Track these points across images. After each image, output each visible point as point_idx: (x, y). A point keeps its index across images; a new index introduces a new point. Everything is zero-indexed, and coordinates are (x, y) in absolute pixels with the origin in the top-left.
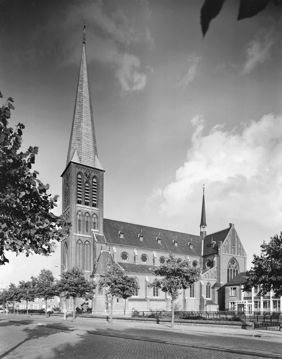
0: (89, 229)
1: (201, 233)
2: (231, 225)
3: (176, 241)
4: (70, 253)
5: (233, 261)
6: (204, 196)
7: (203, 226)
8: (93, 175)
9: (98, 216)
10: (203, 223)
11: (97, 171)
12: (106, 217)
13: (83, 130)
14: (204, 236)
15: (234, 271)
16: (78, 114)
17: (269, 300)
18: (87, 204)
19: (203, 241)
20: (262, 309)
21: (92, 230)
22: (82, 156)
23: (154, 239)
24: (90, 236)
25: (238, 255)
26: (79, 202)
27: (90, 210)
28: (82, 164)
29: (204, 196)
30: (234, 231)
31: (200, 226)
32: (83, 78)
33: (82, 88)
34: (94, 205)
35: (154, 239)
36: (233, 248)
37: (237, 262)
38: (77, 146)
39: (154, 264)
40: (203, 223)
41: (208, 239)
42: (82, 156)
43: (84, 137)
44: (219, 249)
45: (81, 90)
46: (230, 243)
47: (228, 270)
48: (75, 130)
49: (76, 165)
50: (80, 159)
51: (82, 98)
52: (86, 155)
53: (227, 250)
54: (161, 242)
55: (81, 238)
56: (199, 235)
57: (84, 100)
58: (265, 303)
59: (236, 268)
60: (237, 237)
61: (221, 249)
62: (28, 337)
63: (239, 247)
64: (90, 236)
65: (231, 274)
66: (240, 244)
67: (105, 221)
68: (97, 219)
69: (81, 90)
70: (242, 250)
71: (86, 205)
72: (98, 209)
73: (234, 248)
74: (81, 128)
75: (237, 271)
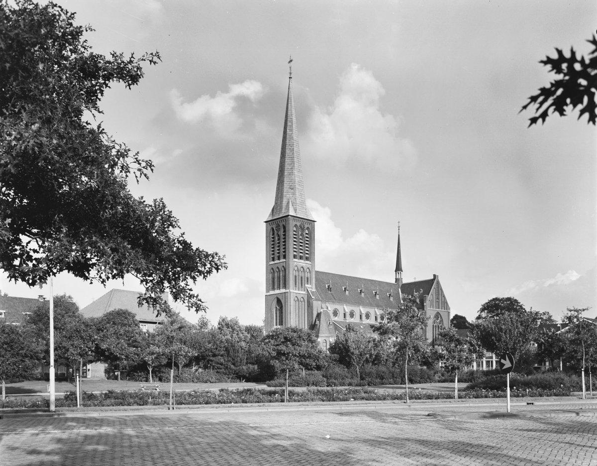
0: (303, 284)
1: (397, 280)
2: (435, 276)
3: (378, 293)
4: (289, 311)
5: (438, 315)
6: (399, 235)
7: (399, 272)
8: (306, 226)
9: (311, 270)
10: (398, 268)
11: (310, 222)
12: (317, 269)
13: (296, 178)
14: (400, 285)
15: (438, 327)
16: (289, 159)
17: (491, 360)
18: (301, 258)
19: (400, 289)
20: (485, 368)
21: (306, 285)
22: (297, 207)
23: (357, 291)
24: (304, 293)
25: (442, 309)
26: (295, 257)
27: (304, 265)
28: (298, 216)
29: (399, 235)
30: (438, 283)
31: (396, 271)
32: (292, 119)
33: (291, 130)
34: (307, 259)
35: (357, 291)
36: (438, 301)
37: (441, 317)
38: (291, 196)
39: (362, 321)
40: (398, 268)
41: (408, 288)
42: (297, 207)
43: (297, 186)
44: (425, 304)
45: (291, 132)
46: (434, 296)
47: (433, 326)
48: (287, 176)
49: (293, 218)
50: (295, 210)
51: (292, 141)
52: (300, 205)
53: (432, 305)
54: (365, 295)
55: (298, 295)
56: (393, 281)
57: (294, 143)
58: (488, 362)
59: (440, 323)
60: (441, 289)
61: (427, 304)
62: (25, 431)
63: (443, 300)
64: (304, 293)
65: (436, 330)
66: (444, 296)
67: (317, 272)
68: (310, 273)
69: (291, 132)
70: (446, 304)
71: (300, 259)
72: (310, 263)
73: (438, 302)
74: (293, 176)
75: (441, 326)
